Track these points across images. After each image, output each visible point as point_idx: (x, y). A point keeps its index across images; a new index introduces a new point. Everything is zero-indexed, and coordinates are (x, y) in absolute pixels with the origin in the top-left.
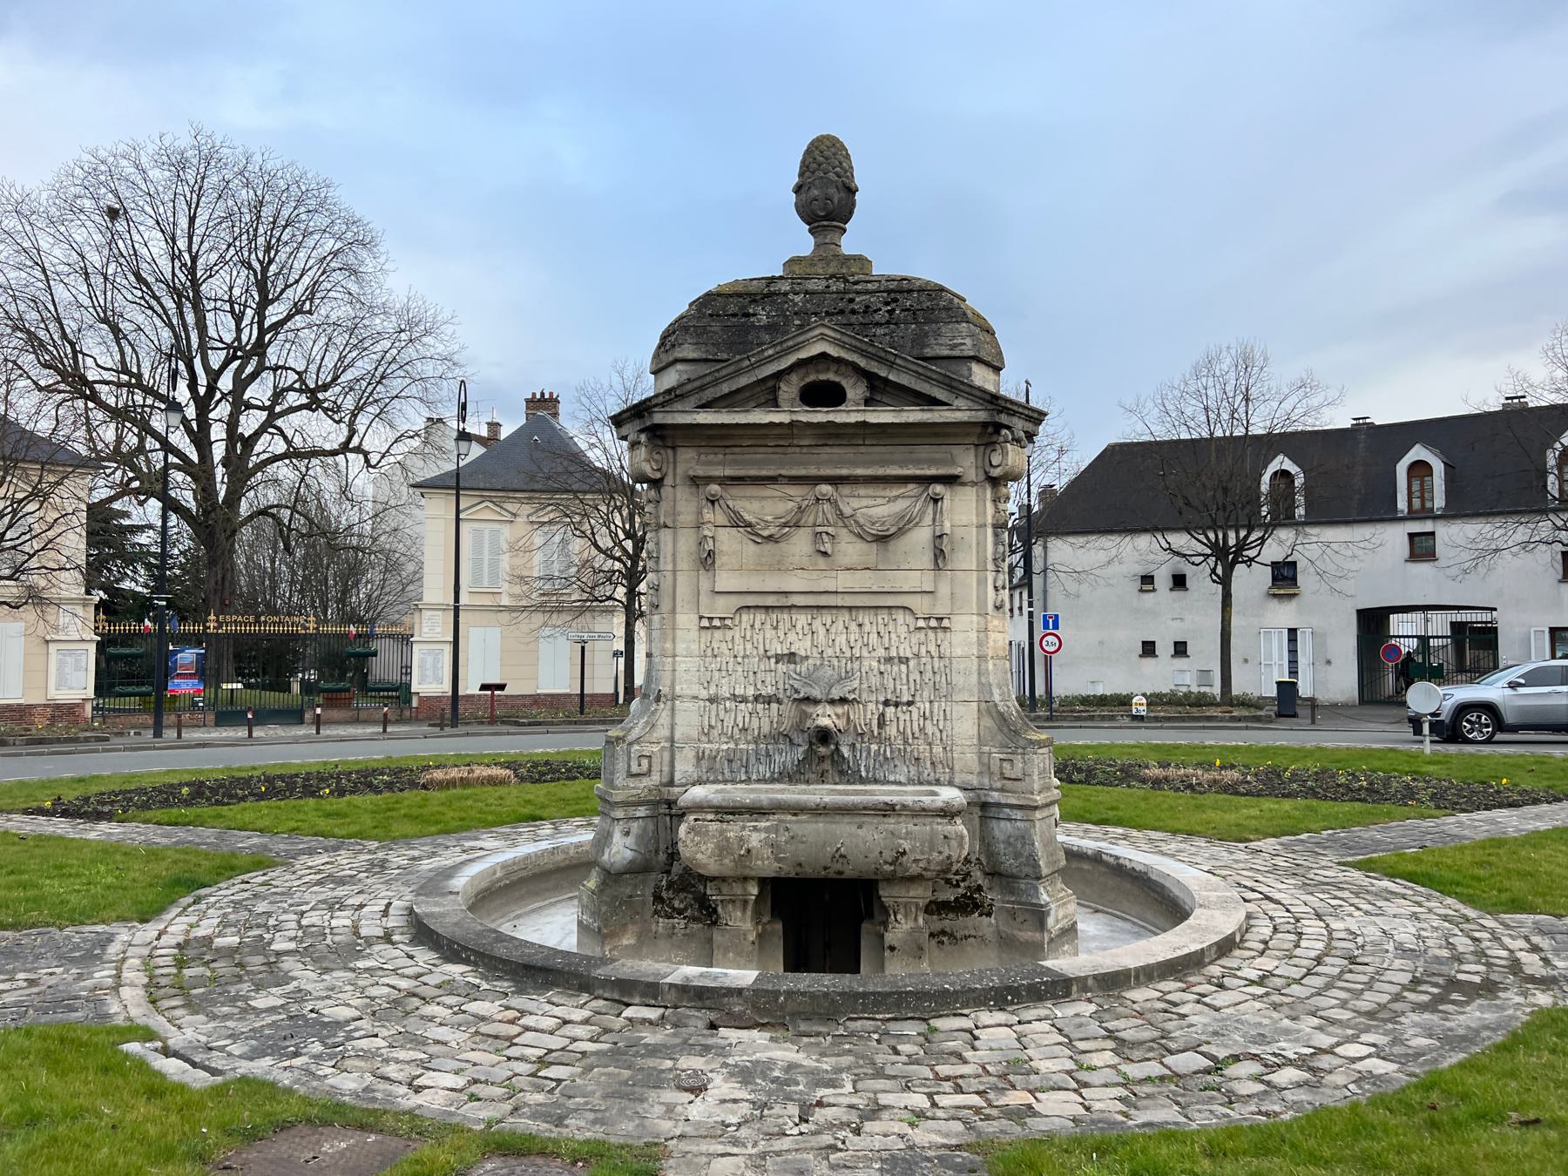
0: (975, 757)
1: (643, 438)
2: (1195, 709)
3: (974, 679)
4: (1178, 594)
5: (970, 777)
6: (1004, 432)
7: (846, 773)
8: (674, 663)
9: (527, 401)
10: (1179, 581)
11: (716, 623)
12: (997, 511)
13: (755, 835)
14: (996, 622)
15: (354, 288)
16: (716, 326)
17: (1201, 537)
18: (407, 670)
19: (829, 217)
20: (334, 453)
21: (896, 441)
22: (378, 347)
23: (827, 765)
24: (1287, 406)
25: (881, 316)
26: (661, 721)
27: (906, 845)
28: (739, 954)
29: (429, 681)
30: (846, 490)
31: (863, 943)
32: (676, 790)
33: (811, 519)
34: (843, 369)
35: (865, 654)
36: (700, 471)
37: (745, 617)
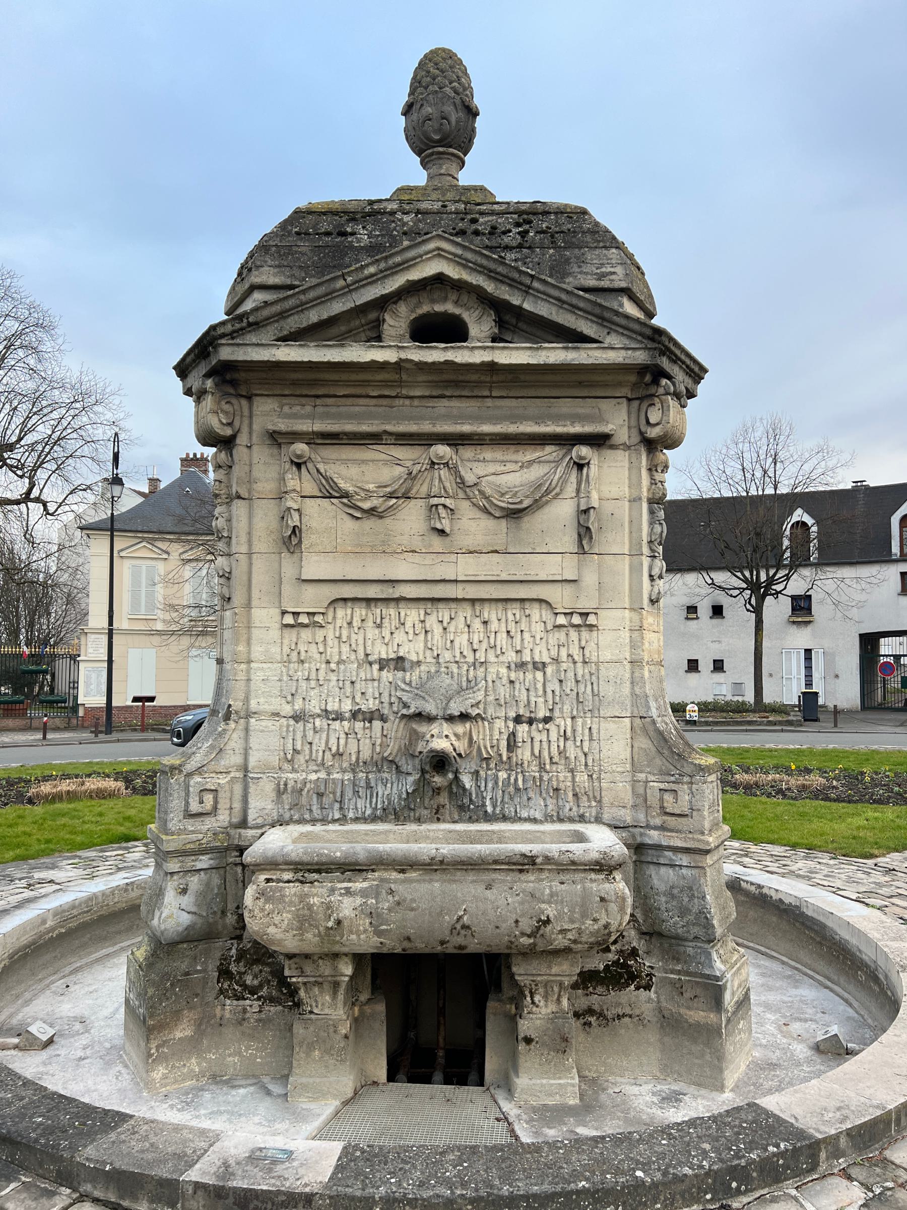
0: (629, 788)
1: (209, 383)
2: (737, 715)
3: (626, 689)
4: (716, 621)
5: (622, 812)
6: (664, 381)
7: (466, 807)
8: (248, 671)
9: (182, 460)
10: (717, 611)
11: (304, 619)
12: (653, 482)
13: (347, 902)
14: (651, 620)
15: (31, 361)
16: (304, 246)
17: (739, 574)
18: (74, 684)
19: (445, 141)
20: (17, 502)
21: (532, 392)
22: (55, 415)
23: (443, 799)
24: (807, 467)
25: (512, 238)
26: (232, 744)
27: (550, 911)
28: (328, 1052)
29: (91, 696)
30: (468, 452)
31: (489, 1026)
32: (250, 833)
33: (424, 490)
34: (465, 298)
35: (492, 658)
36: (282, 425)
37: (340, 613)
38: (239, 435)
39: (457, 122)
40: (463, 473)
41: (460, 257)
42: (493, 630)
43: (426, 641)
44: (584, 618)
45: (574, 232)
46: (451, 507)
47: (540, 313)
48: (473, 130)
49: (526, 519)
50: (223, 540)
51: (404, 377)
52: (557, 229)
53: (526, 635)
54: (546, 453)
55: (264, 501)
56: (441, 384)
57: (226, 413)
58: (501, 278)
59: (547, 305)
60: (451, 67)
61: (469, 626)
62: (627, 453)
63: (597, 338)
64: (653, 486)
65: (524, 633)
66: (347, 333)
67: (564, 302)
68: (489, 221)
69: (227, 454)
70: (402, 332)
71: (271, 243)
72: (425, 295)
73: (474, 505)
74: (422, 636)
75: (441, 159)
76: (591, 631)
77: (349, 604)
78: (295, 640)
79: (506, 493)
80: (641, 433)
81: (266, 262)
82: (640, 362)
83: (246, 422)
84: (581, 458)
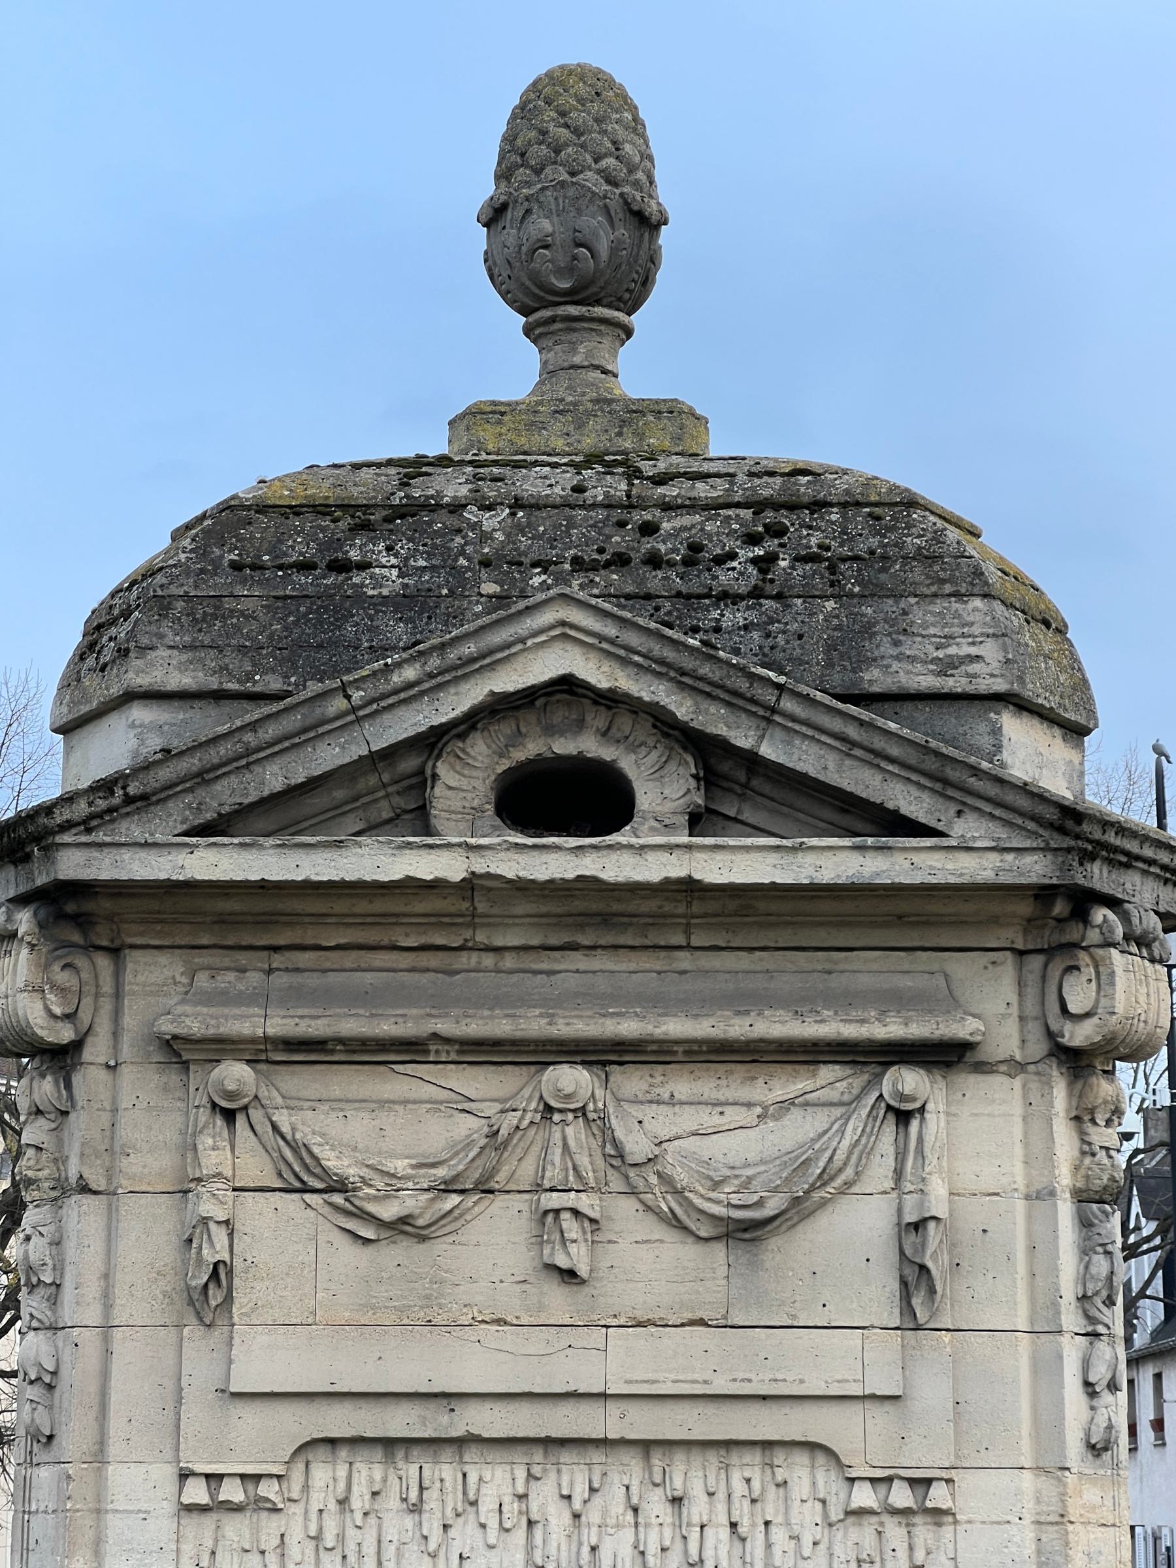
1: (24, 921)
6: (1101, 914)
11: (232, 1492)
14: (1091, 1495)
16: (250, 597)
21: (785, 937)
25: (737, 575)
30: (632, 1081)
33: (527, 1171)
34: (625, 723)
37: (321, 1474)
38: (90, 1040)
39: (614, 249)
40: (620, 1134)
41: (612, 642)
42: (696, 1520)
43: (530, 1548)
44: (920, 1490)
45: (884, 558)
46: (592, 1215)
47: (801, 767)
48: (653, 260)
49: (774, 1243)
50: (41, 1291)
51: (481, 907)
52: (845, 551)
53: (779, 1535)
54: (820, 1082)
55: (144, 1199)
56: (570, 920)
57: (61, 991)
58: (708, 689)
59: (815, 749)
60: (598, 120)
61: (635, 1510)
62: (1017, 1083)
63: (933, 823)
64: (1088, 1160)
65: (773, 1529)
66: (347, 803)
67: (854, 744)
68: (684, 529)
69: (56, 1082)
70: (476, 803)
71: (174, 590)
72: (532, 717)
73: (648, 1208)
74: (520, 1534)
75: (574, 330)
76: (939, 1525)
77: (343, 1453)
78: (209, 1543)
79: (725, 1180)
80: (1051, 1035)
81: (161, 636)
82: (1033, 879)
83: (107, 1006)
84: (903, 1098)
